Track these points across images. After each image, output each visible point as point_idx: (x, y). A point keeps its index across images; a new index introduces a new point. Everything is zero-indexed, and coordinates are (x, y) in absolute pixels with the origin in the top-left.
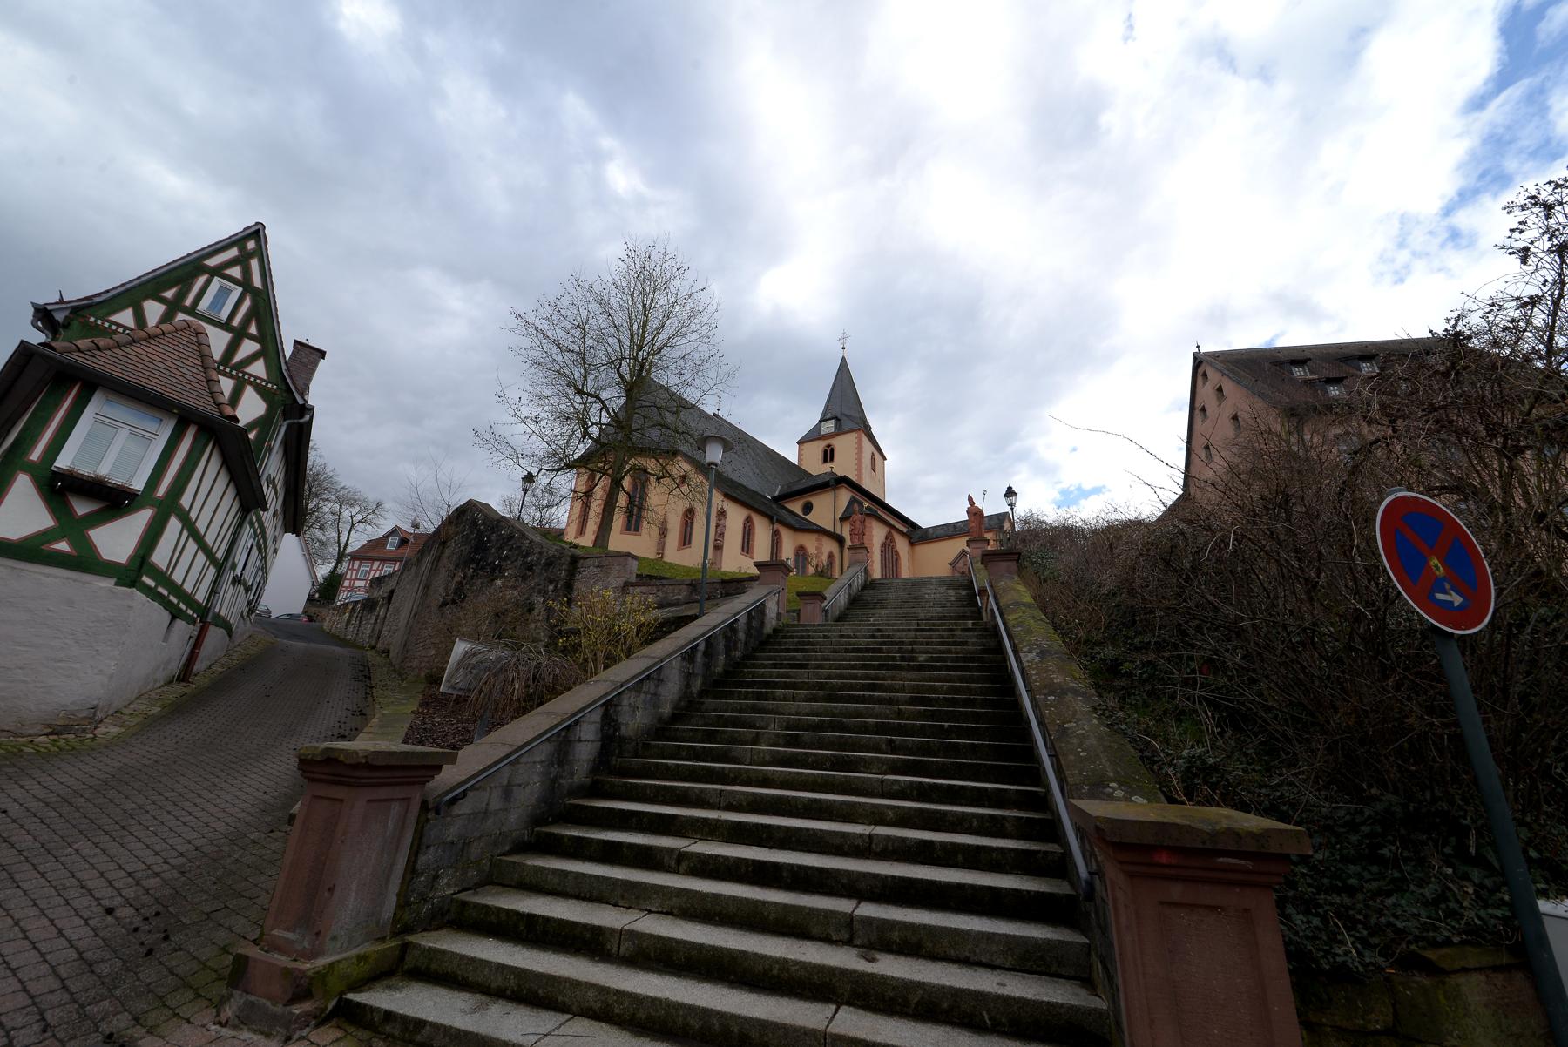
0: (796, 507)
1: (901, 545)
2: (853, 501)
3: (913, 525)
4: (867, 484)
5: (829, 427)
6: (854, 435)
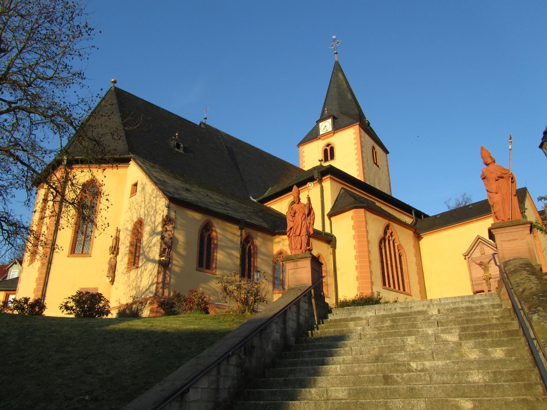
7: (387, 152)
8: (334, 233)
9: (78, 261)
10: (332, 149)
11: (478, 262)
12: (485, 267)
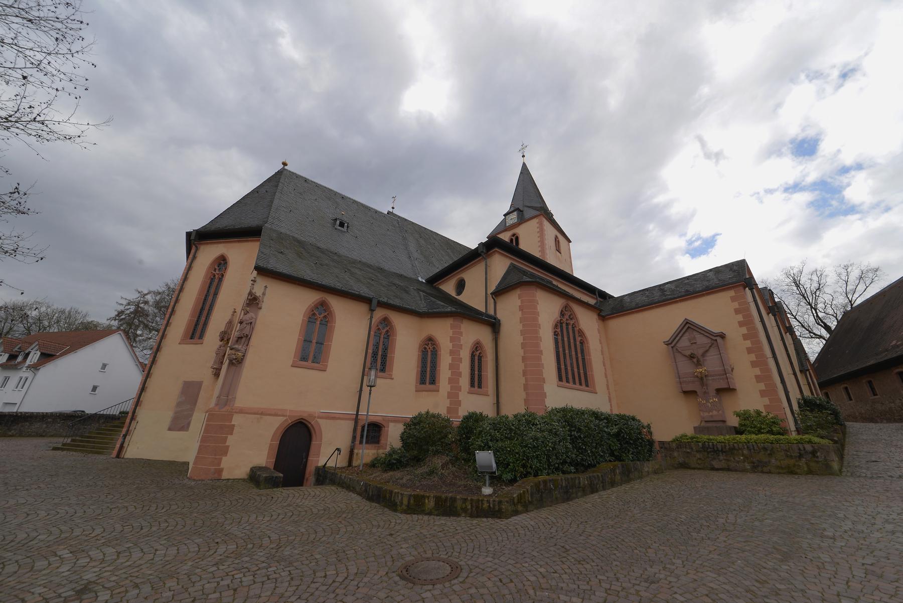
0: (449, 287)
1: (587, 321)
2: (512, 269)
3: (603, 295)
4: (552, 259)
5: (514, 217)
6: (535, 221)
7: (569, 241)
8: (499, 316)
9: (190, 348)
10: (517, 238)
11: (688, 353)
12: (698, 361)
